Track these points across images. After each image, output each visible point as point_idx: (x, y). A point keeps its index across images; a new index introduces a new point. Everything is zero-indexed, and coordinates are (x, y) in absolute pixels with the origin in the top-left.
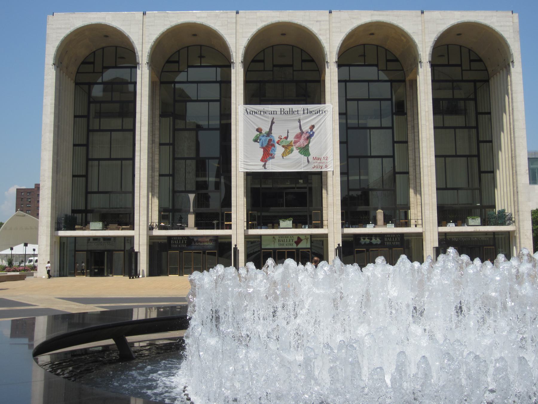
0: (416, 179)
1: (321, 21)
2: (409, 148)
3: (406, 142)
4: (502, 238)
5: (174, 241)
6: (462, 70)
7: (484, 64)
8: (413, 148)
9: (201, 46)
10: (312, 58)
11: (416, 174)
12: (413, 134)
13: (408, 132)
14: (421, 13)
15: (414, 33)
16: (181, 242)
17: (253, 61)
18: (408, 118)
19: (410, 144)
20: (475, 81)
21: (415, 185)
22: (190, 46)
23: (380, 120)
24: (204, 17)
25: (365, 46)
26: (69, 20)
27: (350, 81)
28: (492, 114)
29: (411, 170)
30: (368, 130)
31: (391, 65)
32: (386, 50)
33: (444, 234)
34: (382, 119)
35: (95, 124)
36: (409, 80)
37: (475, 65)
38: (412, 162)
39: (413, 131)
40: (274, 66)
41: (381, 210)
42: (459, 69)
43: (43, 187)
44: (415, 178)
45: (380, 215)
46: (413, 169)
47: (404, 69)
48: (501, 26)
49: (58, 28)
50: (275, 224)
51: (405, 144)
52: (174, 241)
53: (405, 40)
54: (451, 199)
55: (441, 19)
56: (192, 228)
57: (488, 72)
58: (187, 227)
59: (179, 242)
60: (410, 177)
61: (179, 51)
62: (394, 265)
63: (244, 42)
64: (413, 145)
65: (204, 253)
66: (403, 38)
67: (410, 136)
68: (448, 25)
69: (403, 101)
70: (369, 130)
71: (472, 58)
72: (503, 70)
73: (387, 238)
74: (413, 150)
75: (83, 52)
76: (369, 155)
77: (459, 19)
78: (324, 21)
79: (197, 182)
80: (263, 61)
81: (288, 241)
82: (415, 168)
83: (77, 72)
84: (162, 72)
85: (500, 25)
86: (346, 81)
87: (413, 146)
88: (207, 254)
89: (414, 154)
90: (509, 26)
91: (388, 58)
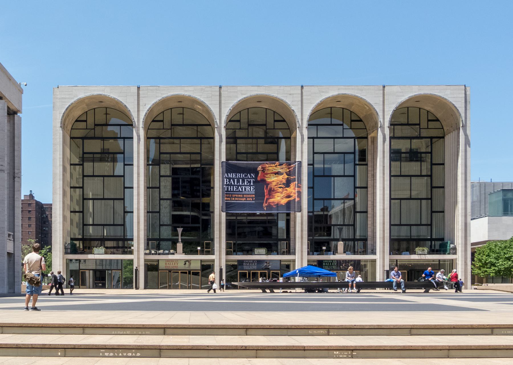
0: (374, 217)
1: (293, 94)
2: (369, 193)
3: (366, 188)
4: (447, 264)
5: (326, 264)
6: (343, 129)
7: (441, 123)
8: (372, 192)
9: (183, 108)
10: (283, 118)
11: (374, 213)
12: (373, 181)
13: (368, 180)
14: (383, 87)
15: (375, 103)
16: (332, 264)
17: (230, 121)
18: (369, 168)
19: (370, 189)
20: (431, 138)
21: (372, 222)
22: (173, 108)
23: (343, 165)
24: (191, 91)
25: (332, 108)
26: (72, 91)
27: (317, 138)
28: (445, 165)
29: (370, 210)
30: (333, 178)
31: (355, 125)
32: (351, 112)
33: (438, 261)
34: (345, 165)
35: (88, 165)
36: (371, 137)
37: (432, 125)
38: (371, 204)
39: (372, 179)
40: (95, 125)
41: (341, 242)
42: (418, 126)
43: (55, 221)
44: (372, 217)
45: (341, 245)
46: (372, 209)
47: (367, 128)
48: (454, 97)
49: (63, 98)
50: (250, 252)
51: (365, 189)
52: (326, 264)
53: (367, 108)
54: (404, 232)
55: (400, 92)
56: (341, 254)
57: (444, 130)
58: (176, 253)
59: (329, 264)
60: (368, 215)
61: (163, 112)
62: (117, 133)
63: (226, 112)
64: (372, 190)
65: (190, 273)
66: (365, 106)
67: (370, 183)
68: (406, 97)
69: (365, 149)
70: (333, 178)
71: (429, 119)
72: (455, 131)
73: (325, 263)
74: (373, 194)
75: (77, 113)
76: (333, 197)
77: (416, 92)
78: (296, 94)
79: (174, 216)
80: (86, 121)
81: (173, 264)
82: (374, 208)
83: (72, 129)
84: (148, 129)
85: (453, 96)
86: (313, 138)
87: (372, 191)
88: (192, 274)
89: (372, 197)
90: (461, 97)
91: (353, 118)
